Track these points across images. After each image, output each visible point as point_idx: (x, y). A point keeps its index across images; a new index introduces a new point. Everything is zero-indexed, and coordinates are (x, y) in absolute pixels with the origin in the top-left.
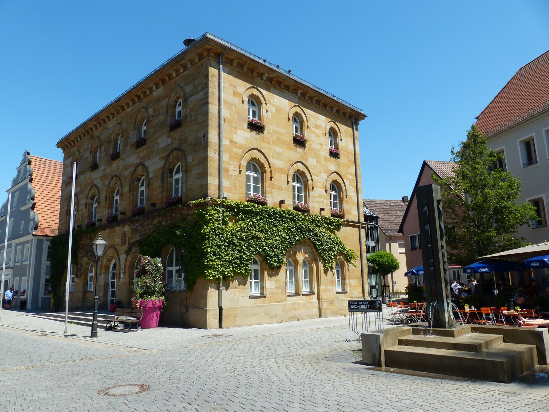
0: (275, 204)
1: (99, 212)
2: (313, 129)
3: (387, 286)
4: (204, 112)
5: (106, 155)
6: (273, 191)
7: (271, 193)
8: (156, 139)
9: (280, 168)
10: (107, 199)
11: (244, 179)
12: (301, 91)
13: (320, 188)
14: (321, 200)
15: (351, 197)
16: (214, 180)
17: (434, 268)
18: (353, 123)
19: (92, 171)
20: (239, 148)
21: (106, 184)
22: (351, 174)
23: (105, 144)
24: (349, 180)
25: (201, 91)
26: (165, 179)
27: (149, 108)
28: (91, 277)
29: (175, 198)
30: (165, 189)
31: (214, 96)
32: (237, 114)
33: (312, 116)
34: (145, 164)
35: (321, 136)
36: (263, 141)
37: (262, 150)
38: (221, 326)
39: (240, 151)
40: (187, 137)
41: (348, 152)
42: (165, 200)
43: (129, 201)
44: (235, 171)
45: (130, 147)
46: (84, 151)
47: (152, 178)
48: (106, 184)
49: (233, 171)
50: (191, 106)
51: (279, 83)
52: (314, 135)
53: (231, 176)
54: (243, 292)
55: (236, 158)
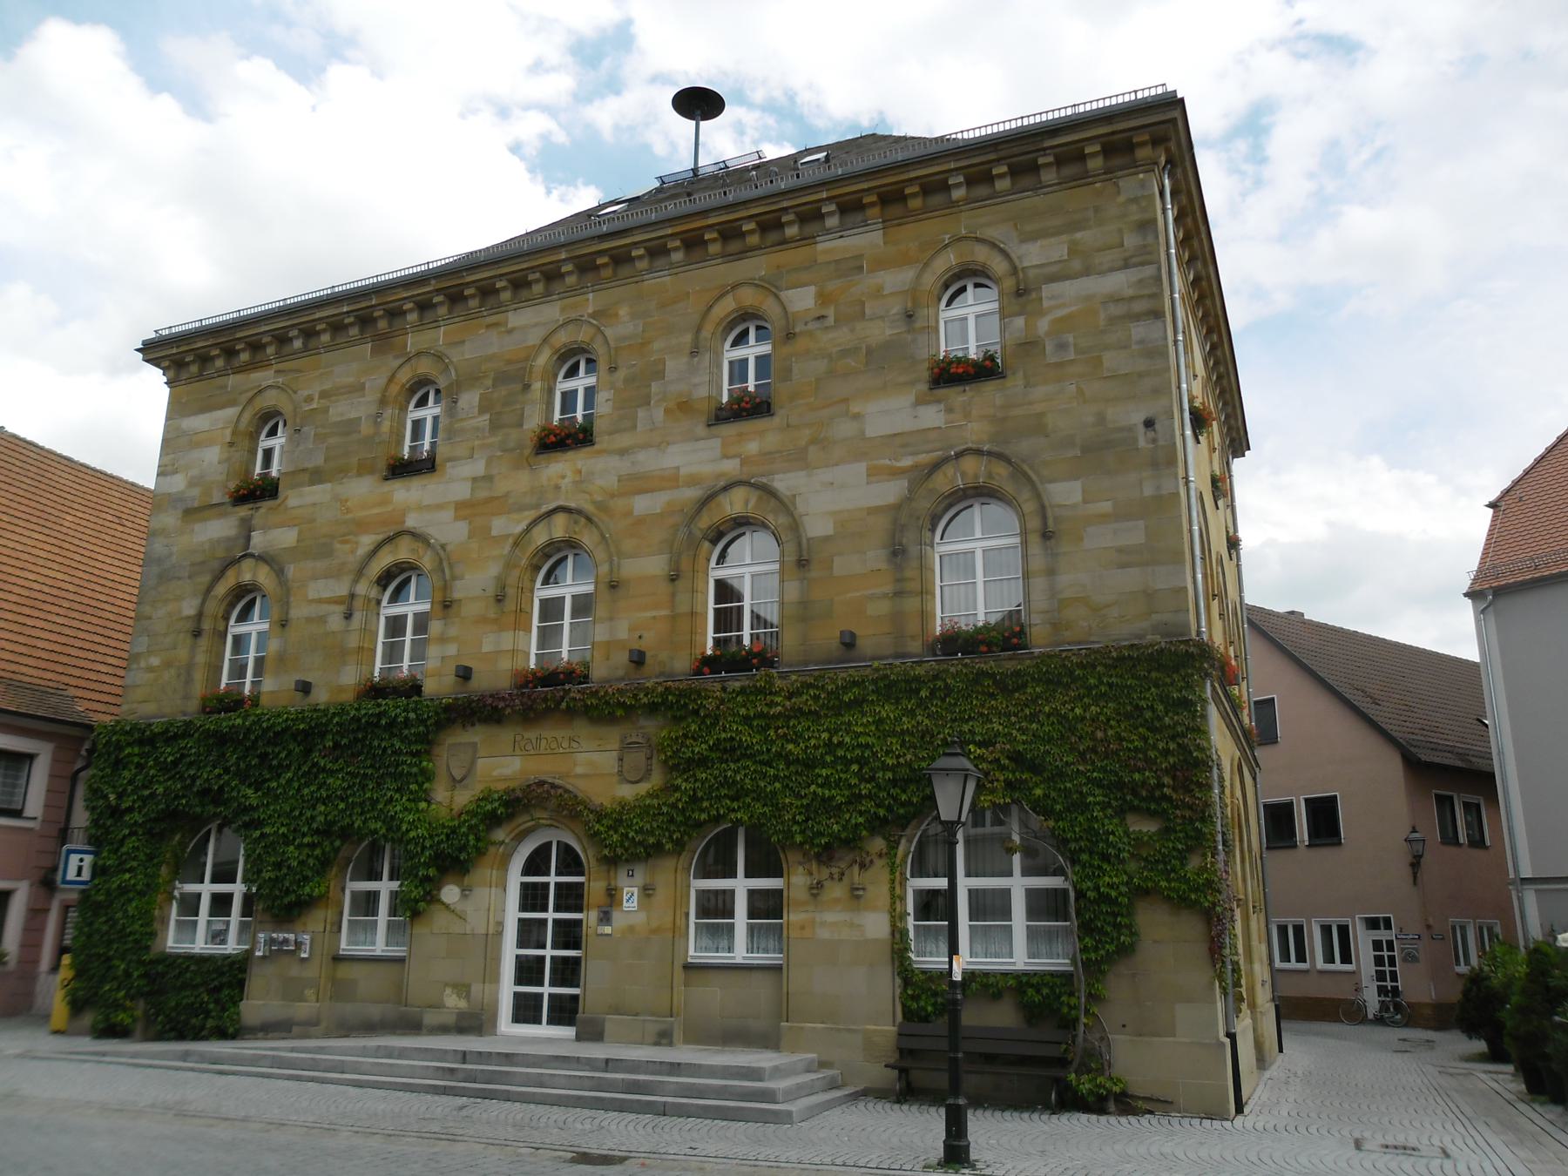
23: (489, 382)
25: (1112, 270)
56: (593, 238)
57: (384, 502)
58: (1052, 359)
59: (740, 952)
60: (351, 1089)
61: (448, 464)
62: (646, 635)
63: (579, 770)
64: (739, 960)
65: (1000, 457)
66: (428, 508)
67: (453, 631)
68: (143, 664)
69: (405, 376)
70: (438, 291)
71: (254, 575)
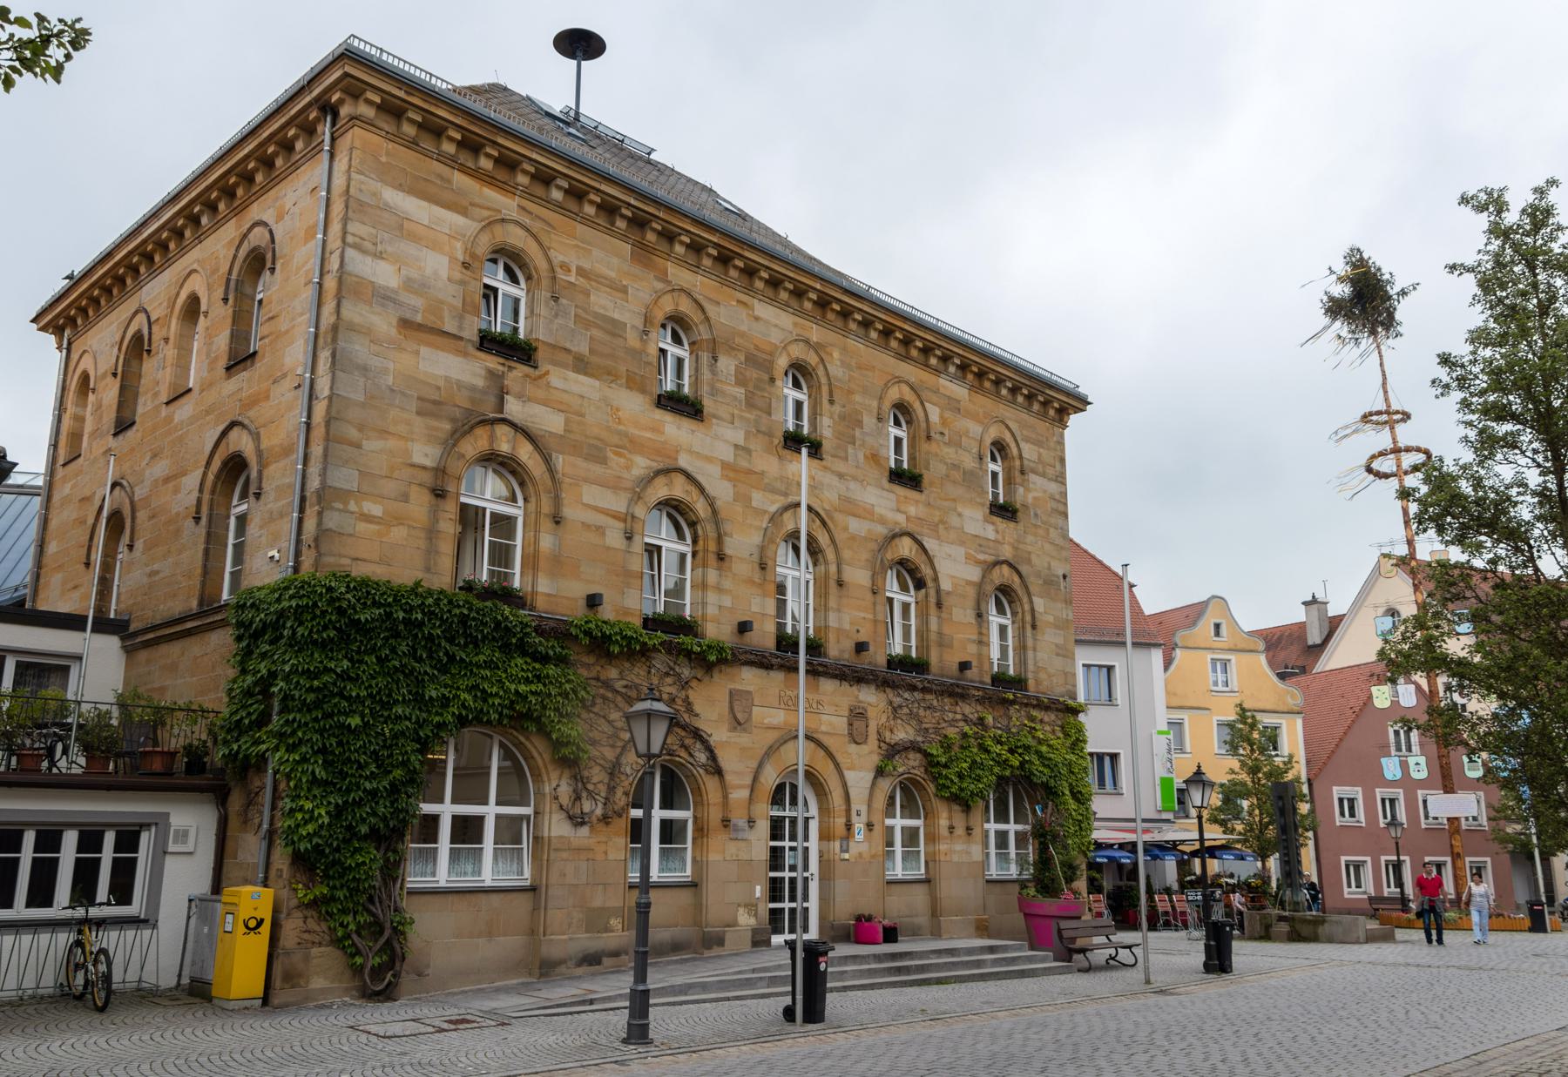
57: (656, 429)
59: (489, 874)
60: (859, 993)
61: (714, 421)
62: (862, 631)
63: (823, 728)
64: (443, 884)
66: (698, 455)
67: (727, 584)
68: (352, 506)
69: (667, 306)
70: (717, 246)
71: (514, 448)
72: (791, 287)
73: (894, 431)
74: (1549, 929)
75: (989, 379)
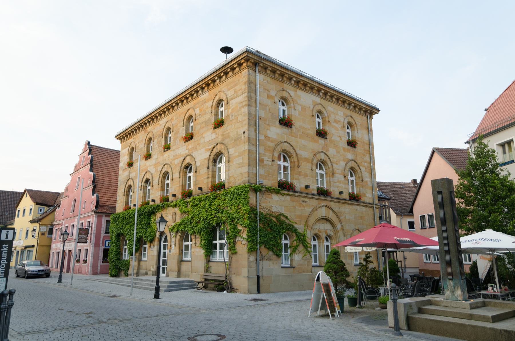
0: (301, 188)
1: (152, 194)
2: (333, 124)
3: (399, 261)
4: (244, 113)
5: (159, 147)
6: (300, 177)
7: (299, 180)
8: (202, 134)
9: (305, 158)
10: (160, 183)
11: (276, 168)
12: (323, 91)
13: (340, 174)
14: (340, 185)
15: (366, 182)
16: (252, 169)
17: (458, 244)
18: (367, 117)
19: (146, 160)
20: (272, 142)
21: (158, 170)
22: (366, 162)
23: (158, 137)
24: (364, 166)
25: (240, 95)
26: (210, 167)
27: (196, 108)
28: (126, 249)
29: (219, 184)
30: (210, 176)
31: (252, 99)
32: (270, 114)
33: (332, 112)
34: (193, 155)
35: (340, 129)
36: (292, 136)
37: (291, 143)
38: (259, 291)
39: (272, 145)
40: (229, 133)
41: (364, 142)
42: (210, 184)
43: (178, 185)
44: (269, 161)
45: (180, 140)
46: (139, 143)
47: (199, 166)
48: (158, 170)
49: (267, 162)
50: (233, 107)
51: (305, 85)
52: (334, 129)
53: (266, 165)
54: (276, 263)
55: (269, 150)
56: (167, 103)
58: (231, 119)
65: (223, 143)
72: (336, 97)
73: (317, 120)
74: (403, 304)
75: (357, 108)
